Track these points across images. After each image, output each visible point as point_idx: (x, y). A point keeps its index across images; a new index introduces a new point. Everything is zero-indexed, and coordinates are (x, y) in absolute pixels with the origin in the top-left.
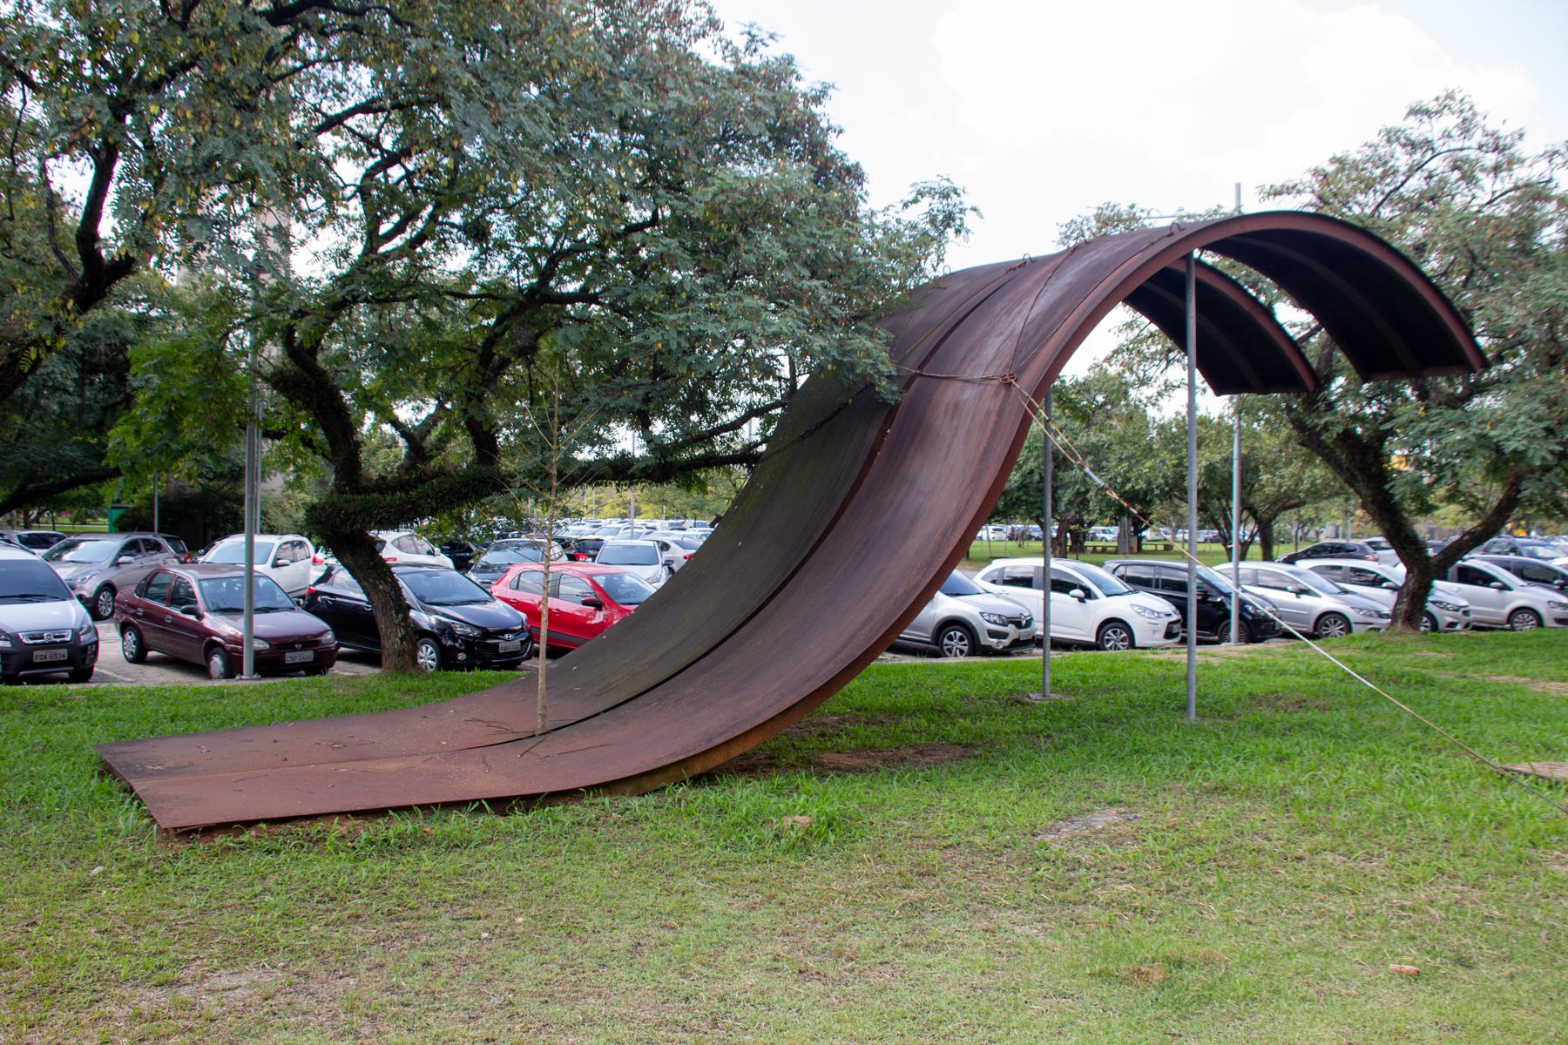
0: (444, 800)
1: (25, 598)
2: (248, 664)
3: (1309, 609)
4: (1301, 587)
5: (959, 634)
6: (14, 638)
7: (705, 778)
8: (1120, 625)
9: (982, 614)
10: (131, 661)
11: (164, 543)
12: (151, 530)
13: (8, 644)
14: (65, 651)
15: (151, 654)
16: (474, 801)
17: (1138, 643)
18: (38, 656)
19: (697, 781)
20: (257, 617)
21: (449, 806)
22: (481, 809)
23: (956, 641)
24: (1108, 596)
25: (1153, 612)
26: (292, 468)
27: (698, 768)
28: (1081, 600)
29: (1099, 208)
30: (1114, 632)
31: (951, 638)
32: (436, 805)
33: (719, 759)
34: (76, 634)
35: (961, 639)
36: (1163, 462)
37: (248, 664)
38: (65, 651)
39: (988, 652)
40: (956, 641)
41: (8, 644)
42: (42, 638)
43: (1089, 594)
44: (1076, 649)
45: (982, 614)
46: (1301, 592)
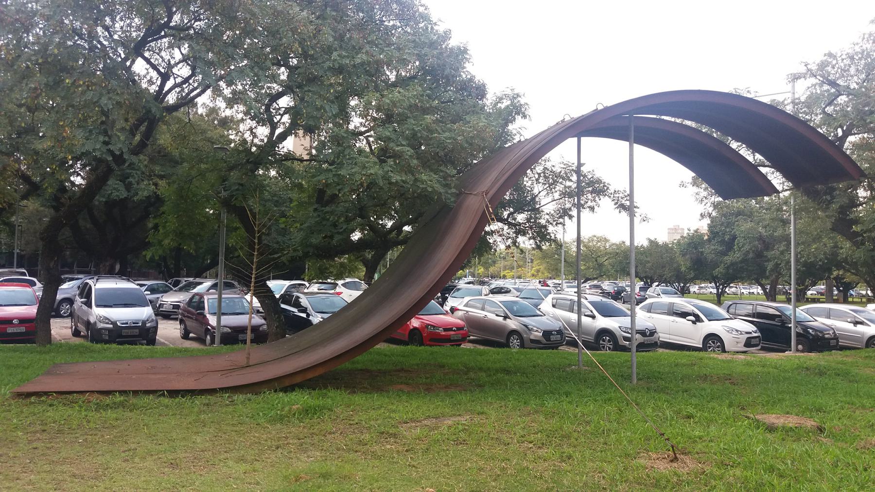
0: (133, 389)
1: (126, 305)
2: (217, 340)
3: (863, 334)
4: (857, 320)
5: (608, 338)
6: (114, 323)
7: (289, 389)
8: (717, 338)
9: (620, 327)
10: (183, 338)
11: (236, 283)
12: (304, 280)
13: (111, 326)
14: (137, 331)
15: (191, 335)
16: (161, 391)
17: (727, 348)
18: (124, 332)
19: (285, 390)
20: (223, 318)
21: (148, 392)
22: (163, 395)
23: (606, 342)
24: (710, 320)
25: (737, 331)
26: (598, 272)
27: (287, 383)
28: (694, 322)
29: (830, 55)
30: (713, 343)
31: (604, 341)
32: (141, 391)
33: (298, 379)
34: (144, 322)
35: (609, 341)
36: (825, 245)
37: (217, 340)
38: (137, 331)
39: (625, 349)
40: (606, 342)
41: (111, 326)
42: (127, 324)
43: (698, 319)
44: (693, 351)
45: (620, 327)
46: (856, 323)
